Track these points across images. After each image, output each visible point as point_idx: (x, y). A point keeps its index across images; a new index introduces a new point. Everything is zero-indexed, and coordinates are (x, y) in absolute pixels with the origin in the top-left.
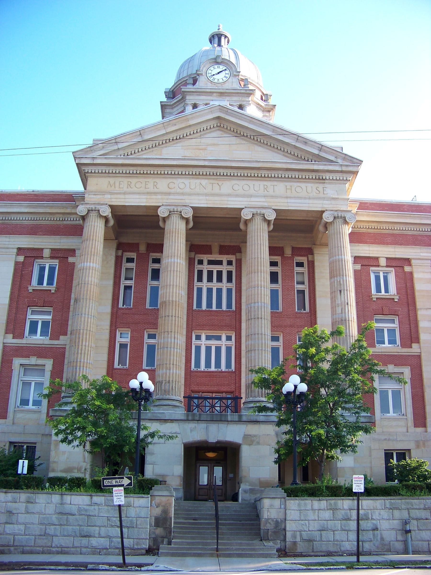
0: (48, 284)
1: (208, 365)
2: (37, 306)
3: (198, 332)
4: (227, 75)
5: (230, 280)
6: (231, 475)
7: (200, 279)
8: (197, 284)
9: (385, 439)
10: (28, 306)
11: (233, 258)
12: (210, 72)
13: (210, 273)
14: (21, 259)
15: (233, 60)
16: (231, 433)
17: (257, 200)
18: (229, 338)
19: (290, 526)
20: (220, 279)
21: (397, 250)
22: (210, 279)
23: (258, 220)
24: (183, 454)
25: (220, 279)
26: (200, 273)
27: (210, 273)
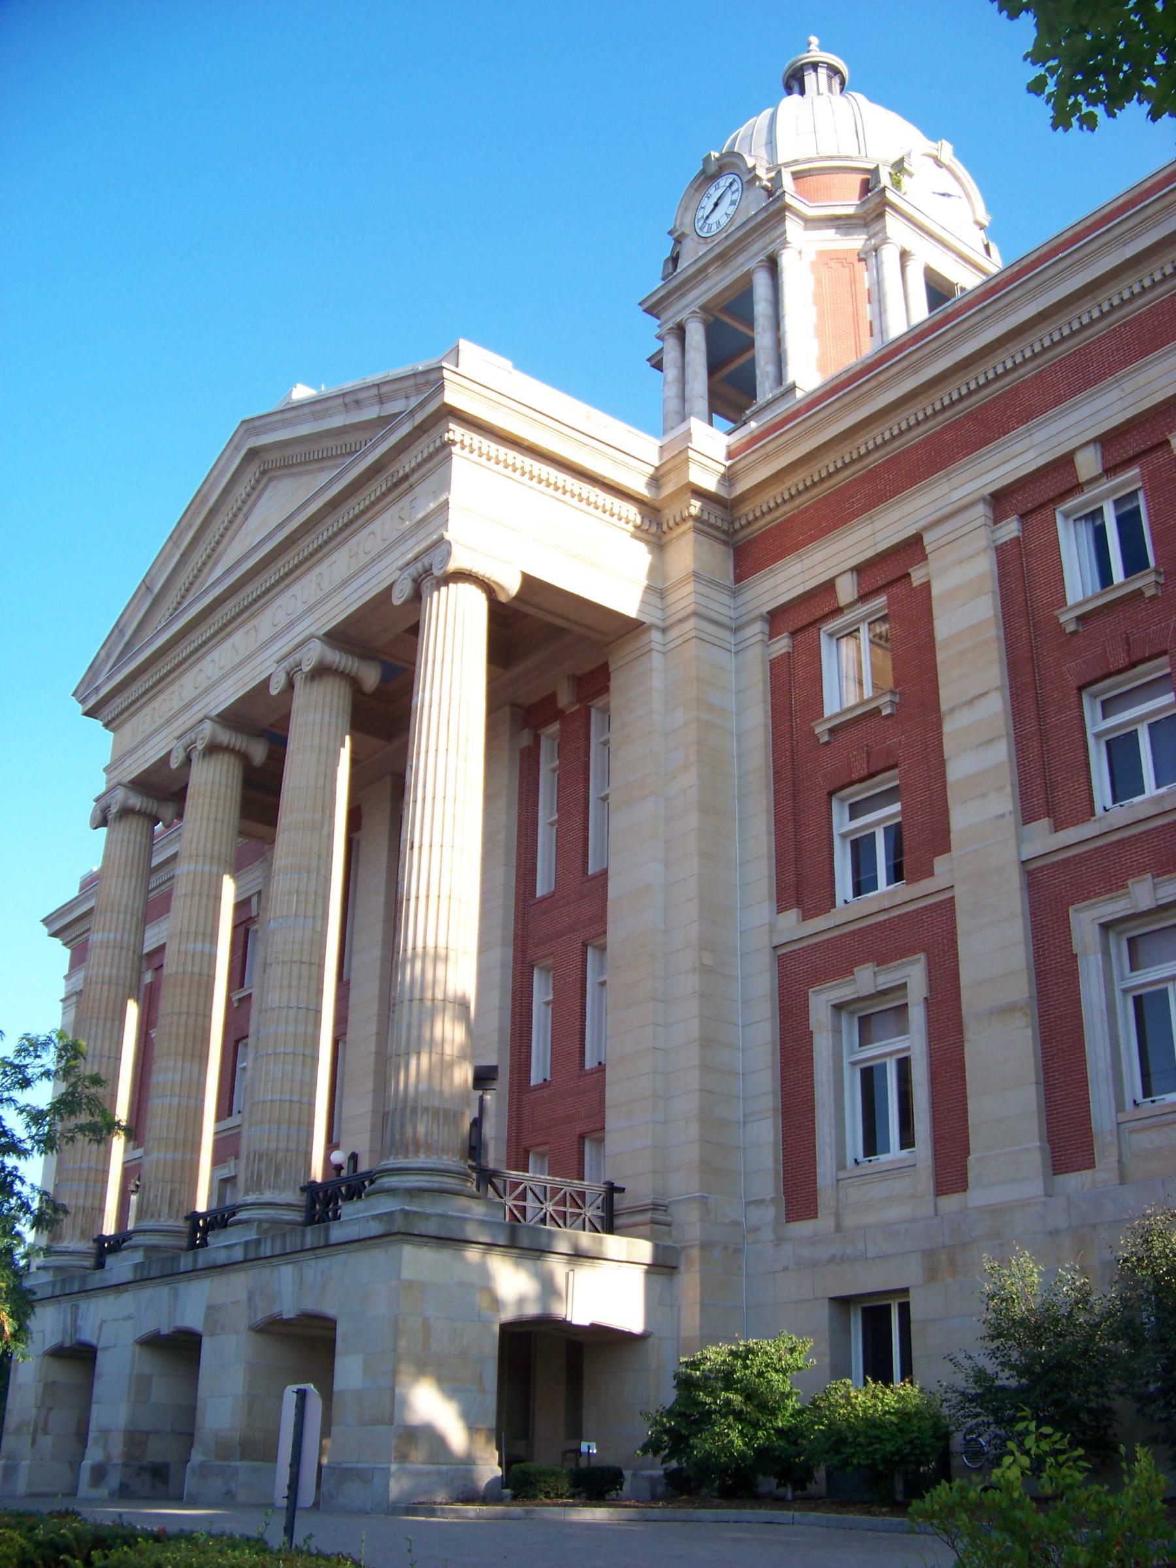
0: (1128, 572)
2: (1110, 675)
9: (832, 1260)
10: (1080, 689)
14: (1011, 529)
21: (879, 524)
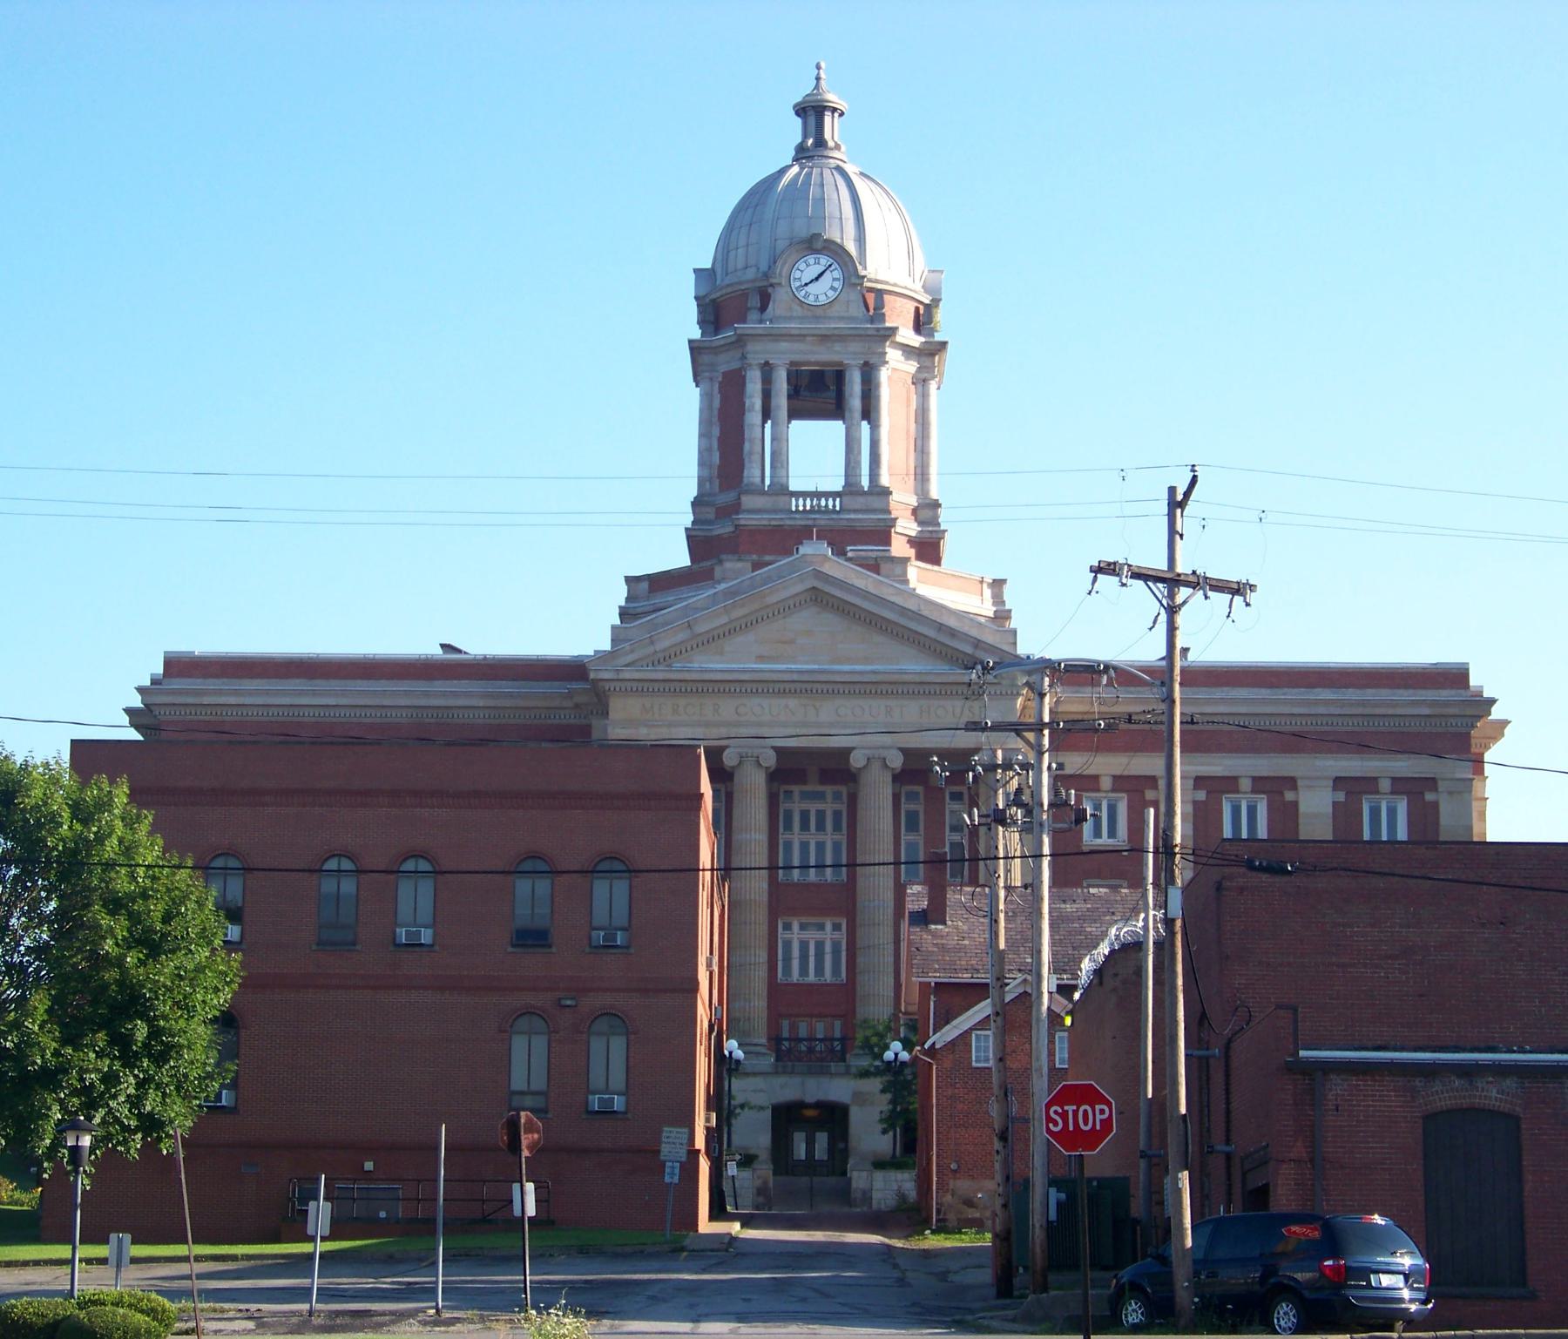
1: (804, 970)
3: (787, 919)
4: (836, 284)
5: (837, 827)
6: (841, 1145)
7: (788, 826)
8: (783, 837)
11: (844, 790)
12: (797, 274)
13: (805, 816)
15: (851, 247)
16: (837, 1089)
17: (871, 732)
18: (836, 927)
19: (876, 1195)
20: (821, 827)
22: (805, 826)
23: (876, 766)
24: (870, 1330)
25: (821, 827)
26: (789, 816)
27: (805, 816)
